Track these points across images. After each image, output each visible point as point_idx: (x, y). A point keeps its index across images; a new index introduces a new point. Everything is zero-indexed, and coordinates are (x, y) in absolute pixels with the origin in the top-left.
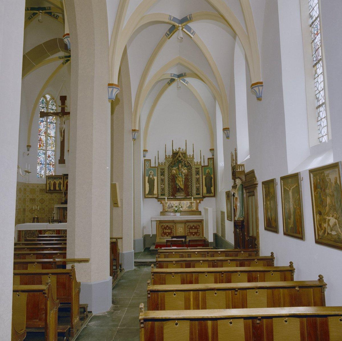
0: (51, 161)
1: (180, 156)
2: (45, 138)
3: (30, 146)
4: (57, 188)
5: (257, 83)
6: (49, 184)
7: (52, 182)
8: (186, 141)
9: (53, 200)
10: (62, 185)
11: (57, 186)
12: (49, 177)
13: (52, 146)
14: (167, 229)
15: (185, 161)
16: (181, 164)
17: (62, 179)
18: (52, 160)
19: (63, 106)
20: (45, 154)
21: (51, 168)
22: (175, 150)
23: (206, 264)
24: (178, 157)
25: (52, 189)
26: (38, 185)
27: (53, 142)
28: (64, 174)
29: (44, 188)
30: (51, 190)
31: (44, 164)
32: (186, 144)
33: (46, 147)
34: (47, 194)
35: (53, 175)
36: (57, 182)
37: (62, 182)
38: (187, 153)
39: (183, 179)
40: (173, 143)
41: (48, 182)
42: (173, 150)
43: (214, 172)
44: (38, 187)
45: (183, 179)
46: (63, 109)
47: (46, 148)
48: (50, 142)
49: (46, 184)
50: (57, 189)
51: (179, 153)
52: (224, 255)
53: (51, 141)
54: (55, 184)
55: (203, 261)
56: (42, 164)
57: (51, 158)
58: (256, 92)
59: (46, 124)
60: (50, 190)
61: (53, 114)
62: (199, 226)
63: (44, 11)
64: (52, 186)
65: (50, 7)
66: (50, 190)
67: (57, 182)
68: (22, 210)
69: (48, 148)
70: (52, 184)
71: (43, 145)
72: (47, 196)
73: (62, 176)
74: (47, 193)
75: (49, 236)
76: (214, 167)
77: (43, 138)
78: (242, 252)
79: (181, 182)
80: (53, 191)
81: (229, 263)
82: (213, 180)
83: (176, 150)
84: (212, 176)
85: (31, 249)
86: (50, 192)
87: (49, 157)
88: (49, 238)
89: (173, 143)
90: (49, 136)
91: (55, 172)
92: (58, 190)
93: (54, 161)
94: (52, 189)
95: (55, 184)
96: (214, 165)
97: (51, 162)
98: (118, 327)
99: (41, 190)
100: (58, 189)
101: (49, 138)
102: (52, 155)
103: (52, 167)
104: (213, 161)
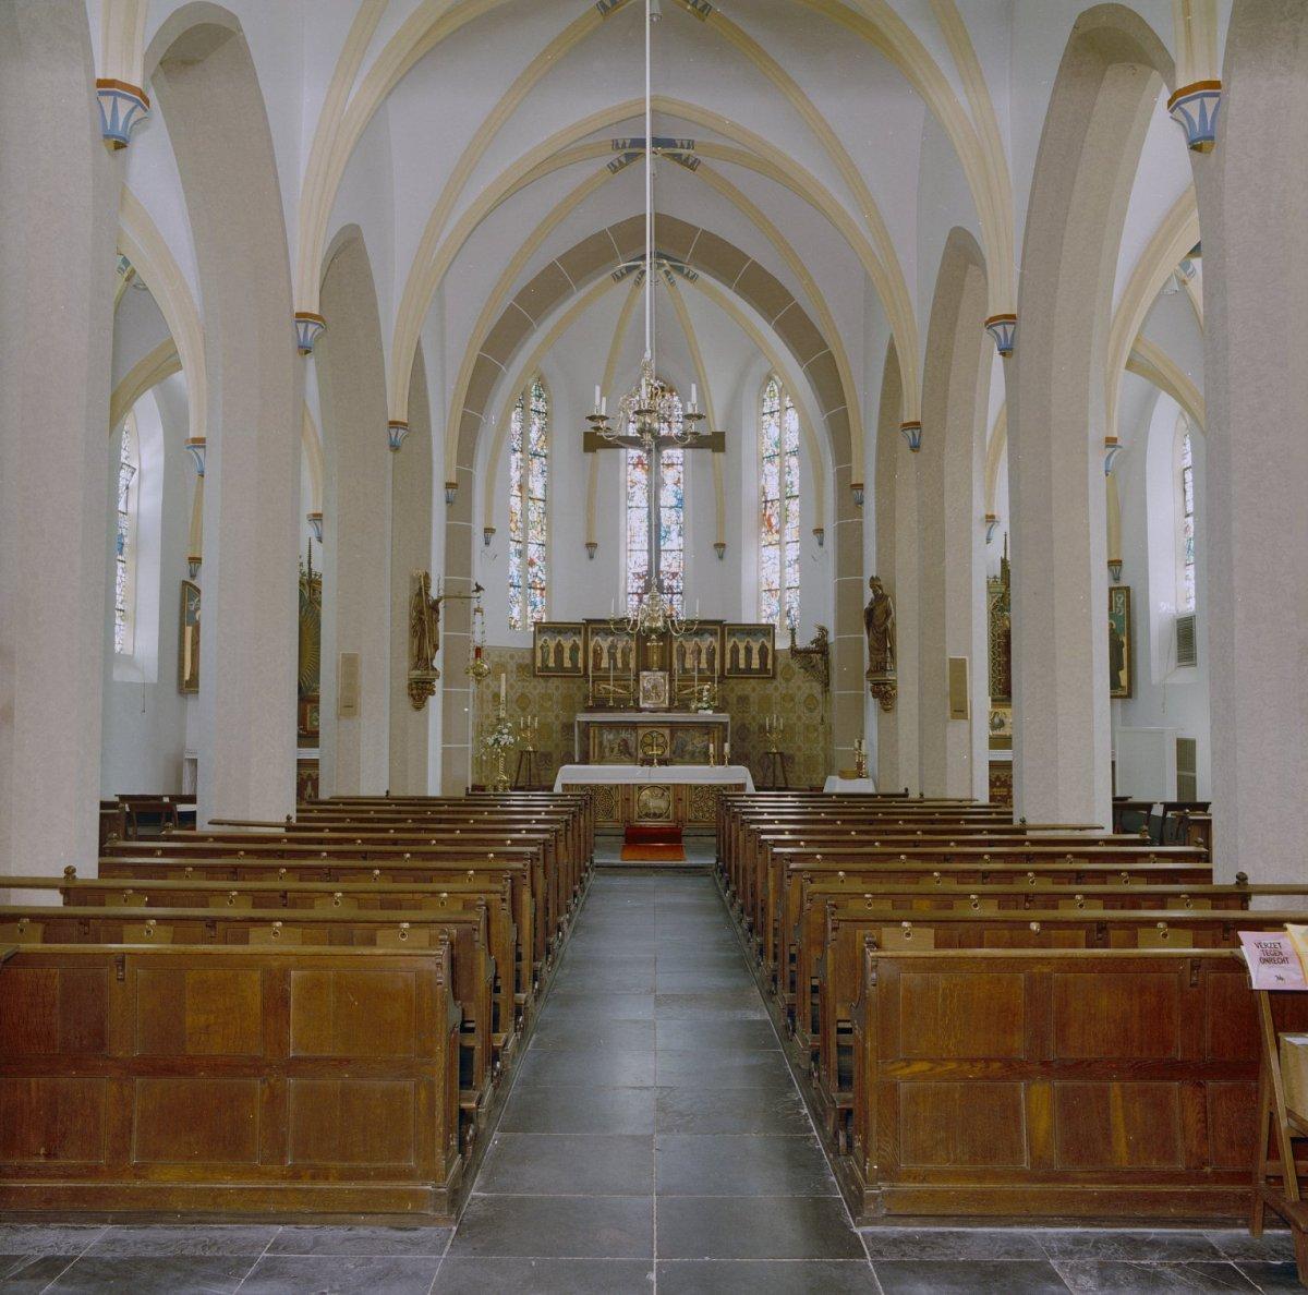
2: (519, 504)
3: (723, 545)
4: (567, 663)
5: (1006, 316)
6: (542, 647)
7: (552, 644)
9: (551, 699)
10: (581, 654)
11: (567, 654)
12: (542, 628)
14: (999, 787)
17: (580, 633)
18: (540, 574)
20: (520, 554)
21: (538, 599)
23: (1188, 934)
26: (513, 653)
27: (542, 516)
28: (587, 621)
29: (528, 661)
30: (547, 666)
31: (519, 587)
33: (525, 531)
34: (535, 682)
35: (544, 621)
36: (567, 645)
37: (581, 644)
41: (540, 643)
43: (1129, 628)
44: (512, 657)
47: (526, 535)
48: (533, 516)
49: (534, 649)
50: (602, 666)
54: (559, 650)
55: (912, 921)
56: (515, 587)
58: (998, 336)
59: (521, 460)
60: (545, 667)
63: (667, 151)
64: (552, 655)
65: (693, 142)
66: (545, 667)
67: (567, 645)
68: (557, 726)
69: (532, 533)
70: (552, 650)
72: (535, 687)
74: (535, 676)
75: (162, 849)
76: (1129, 612)
77: (515, 503)
78: (905, 924)
80: (743, 671)
81: (908, 935)
82: (1125, 649)
84: (1125, 640)
85: (156, 898)
86: (545, 673)
87: (532, 563)
88: (162, 856)
90: (531, 499)
91: (548, 610)
93: (544, 577)
94: (551, 664)
95: (559, 650)
96: (1128, 606)
98: (264, 1254)
99: (521, 668)
100: (570, 666)
101: (531, 503)
102: (539, 558)
103: (541, 595)
104: (1128, 597)
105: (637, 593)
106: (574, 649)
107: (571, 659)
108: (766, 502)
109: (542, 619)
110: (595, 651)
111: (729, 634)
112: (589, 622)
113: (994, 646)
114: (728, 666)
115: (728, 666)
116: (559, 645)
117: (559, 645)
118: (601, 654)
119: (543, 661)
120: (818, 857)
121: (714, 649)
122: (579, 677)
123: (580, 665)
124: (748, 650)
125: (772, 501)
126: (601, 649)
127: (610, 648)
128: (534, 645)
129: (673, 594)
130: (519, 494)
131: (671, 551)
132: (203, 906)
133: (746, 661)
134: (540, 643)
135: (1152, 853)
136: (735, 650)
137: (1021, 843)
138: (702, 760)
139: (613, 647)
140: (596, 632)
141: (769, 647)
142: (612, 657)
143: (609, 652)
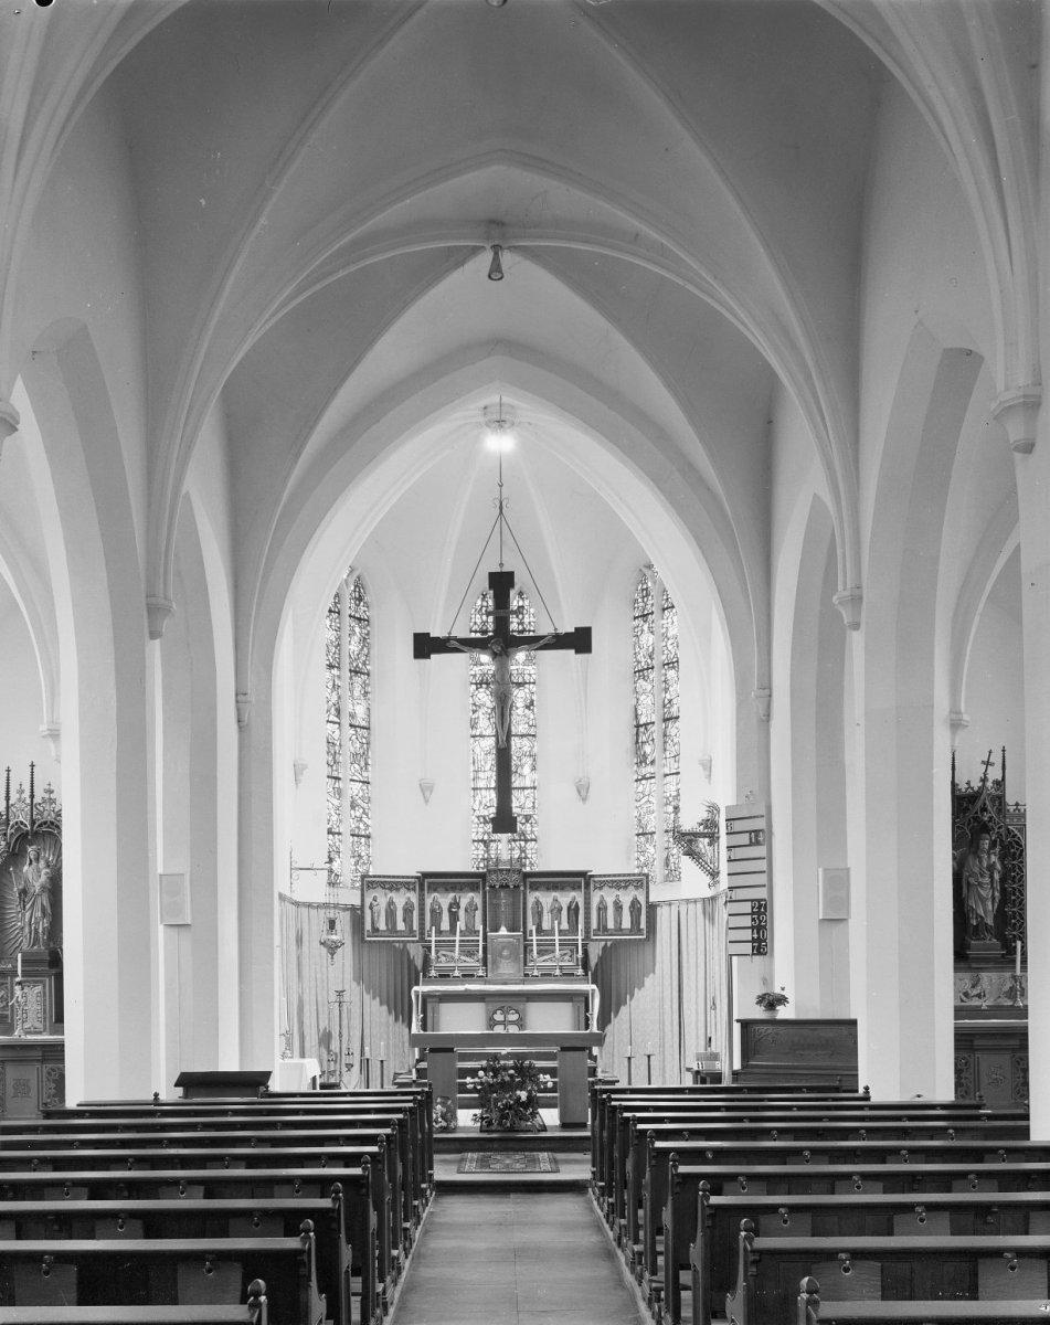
0: (361, 820)
1: (984, 809)
7: (383, 902)
8: (1004, 751)
13: (363, 764)
15: (999, 828)
16: (988, 836)
17: (580, 887)
19: (501, 613)
22: (963, 787)
23: (944, 1219)
24: (976, 813)
25: (382, 926)
30: (378, 930)
32: (32, 775)
37: (580, 901)
38: (1007, 795)
39: (997, 894)
40: (1004, 757)
42: (953, 784)
45: (997, 894)
46: (502, 623)
51: (982, 798)
52: (244, 1163)
53: (358, 745)
54: (618, 907)
57: (361, 810)
61: (463, 644)
62: (53, 1070)
71: (334, 758)
73: (417, 877)
79: (990, 903)
83: (968, 783)
89: (1004, 757)
92: (401, 931)
97: (361, 826)
105: (482, 841)
106: (408, 910)
107: (404, 920)
108: (638, 726)
109: (529, 661)
110: (433, 911)
111: (429, 888)
112: (426, 875)
113: (1021, 855)
114: (594, 925)
115: (594, 925)
116: (391, 903)
117: (391, 903)
118: (440, 914)
119: (373, 923)
120: (951, 1131)
121: (412, 906)
122: (413, 942)
123: (416, 927)
124: (618, 907)
125: (646, 725)
126: (440, 907)
127: (451, 906)
128: (363, 900)
129: (526, 841)
130: (336, 720)
131: (524, 788)
132: (1024, 1047)
133: (616, 921)
134: (368, 901)
135: (904, 1148)
136: (602, 909)
137: (978, 1118)
138: (126, 1194)
139: (455, 904)
140: (434, 888)
141: (642, 899)
142: (454, 918)
143: (450, 911)
